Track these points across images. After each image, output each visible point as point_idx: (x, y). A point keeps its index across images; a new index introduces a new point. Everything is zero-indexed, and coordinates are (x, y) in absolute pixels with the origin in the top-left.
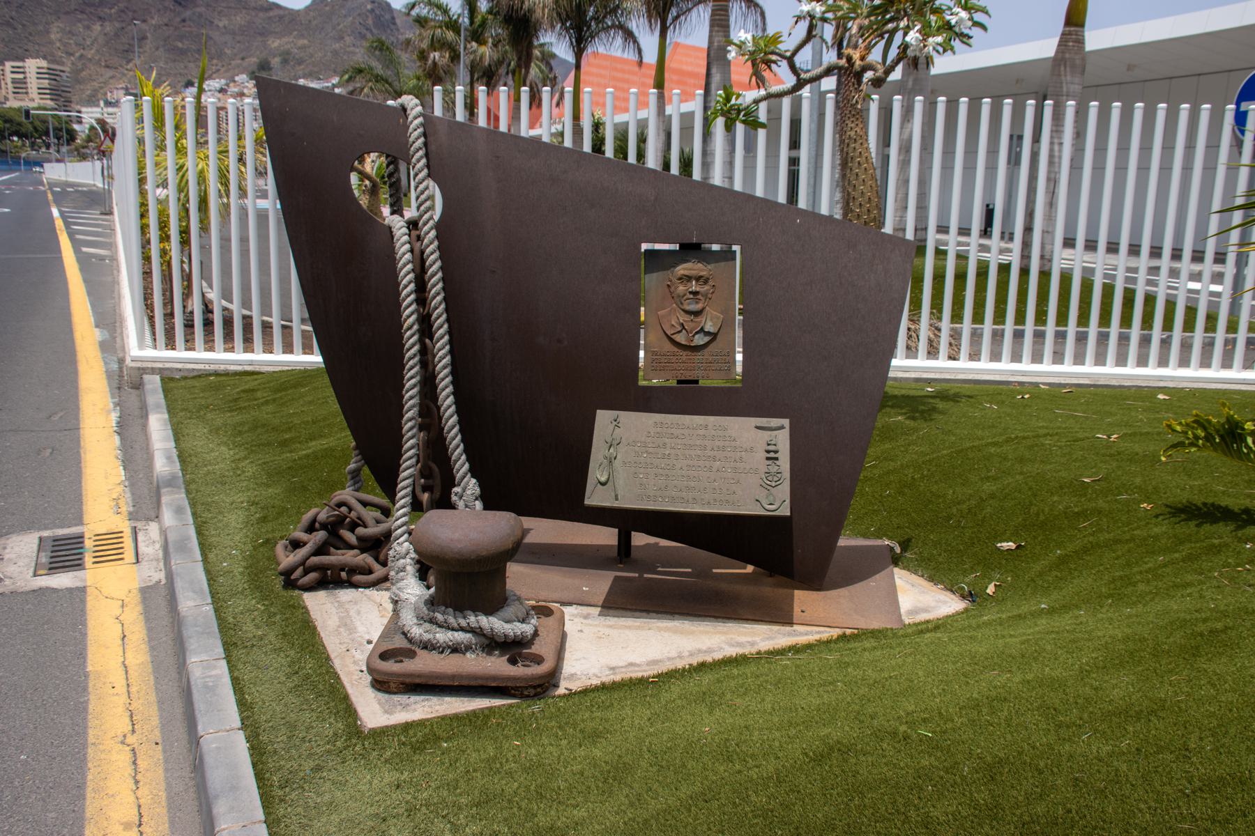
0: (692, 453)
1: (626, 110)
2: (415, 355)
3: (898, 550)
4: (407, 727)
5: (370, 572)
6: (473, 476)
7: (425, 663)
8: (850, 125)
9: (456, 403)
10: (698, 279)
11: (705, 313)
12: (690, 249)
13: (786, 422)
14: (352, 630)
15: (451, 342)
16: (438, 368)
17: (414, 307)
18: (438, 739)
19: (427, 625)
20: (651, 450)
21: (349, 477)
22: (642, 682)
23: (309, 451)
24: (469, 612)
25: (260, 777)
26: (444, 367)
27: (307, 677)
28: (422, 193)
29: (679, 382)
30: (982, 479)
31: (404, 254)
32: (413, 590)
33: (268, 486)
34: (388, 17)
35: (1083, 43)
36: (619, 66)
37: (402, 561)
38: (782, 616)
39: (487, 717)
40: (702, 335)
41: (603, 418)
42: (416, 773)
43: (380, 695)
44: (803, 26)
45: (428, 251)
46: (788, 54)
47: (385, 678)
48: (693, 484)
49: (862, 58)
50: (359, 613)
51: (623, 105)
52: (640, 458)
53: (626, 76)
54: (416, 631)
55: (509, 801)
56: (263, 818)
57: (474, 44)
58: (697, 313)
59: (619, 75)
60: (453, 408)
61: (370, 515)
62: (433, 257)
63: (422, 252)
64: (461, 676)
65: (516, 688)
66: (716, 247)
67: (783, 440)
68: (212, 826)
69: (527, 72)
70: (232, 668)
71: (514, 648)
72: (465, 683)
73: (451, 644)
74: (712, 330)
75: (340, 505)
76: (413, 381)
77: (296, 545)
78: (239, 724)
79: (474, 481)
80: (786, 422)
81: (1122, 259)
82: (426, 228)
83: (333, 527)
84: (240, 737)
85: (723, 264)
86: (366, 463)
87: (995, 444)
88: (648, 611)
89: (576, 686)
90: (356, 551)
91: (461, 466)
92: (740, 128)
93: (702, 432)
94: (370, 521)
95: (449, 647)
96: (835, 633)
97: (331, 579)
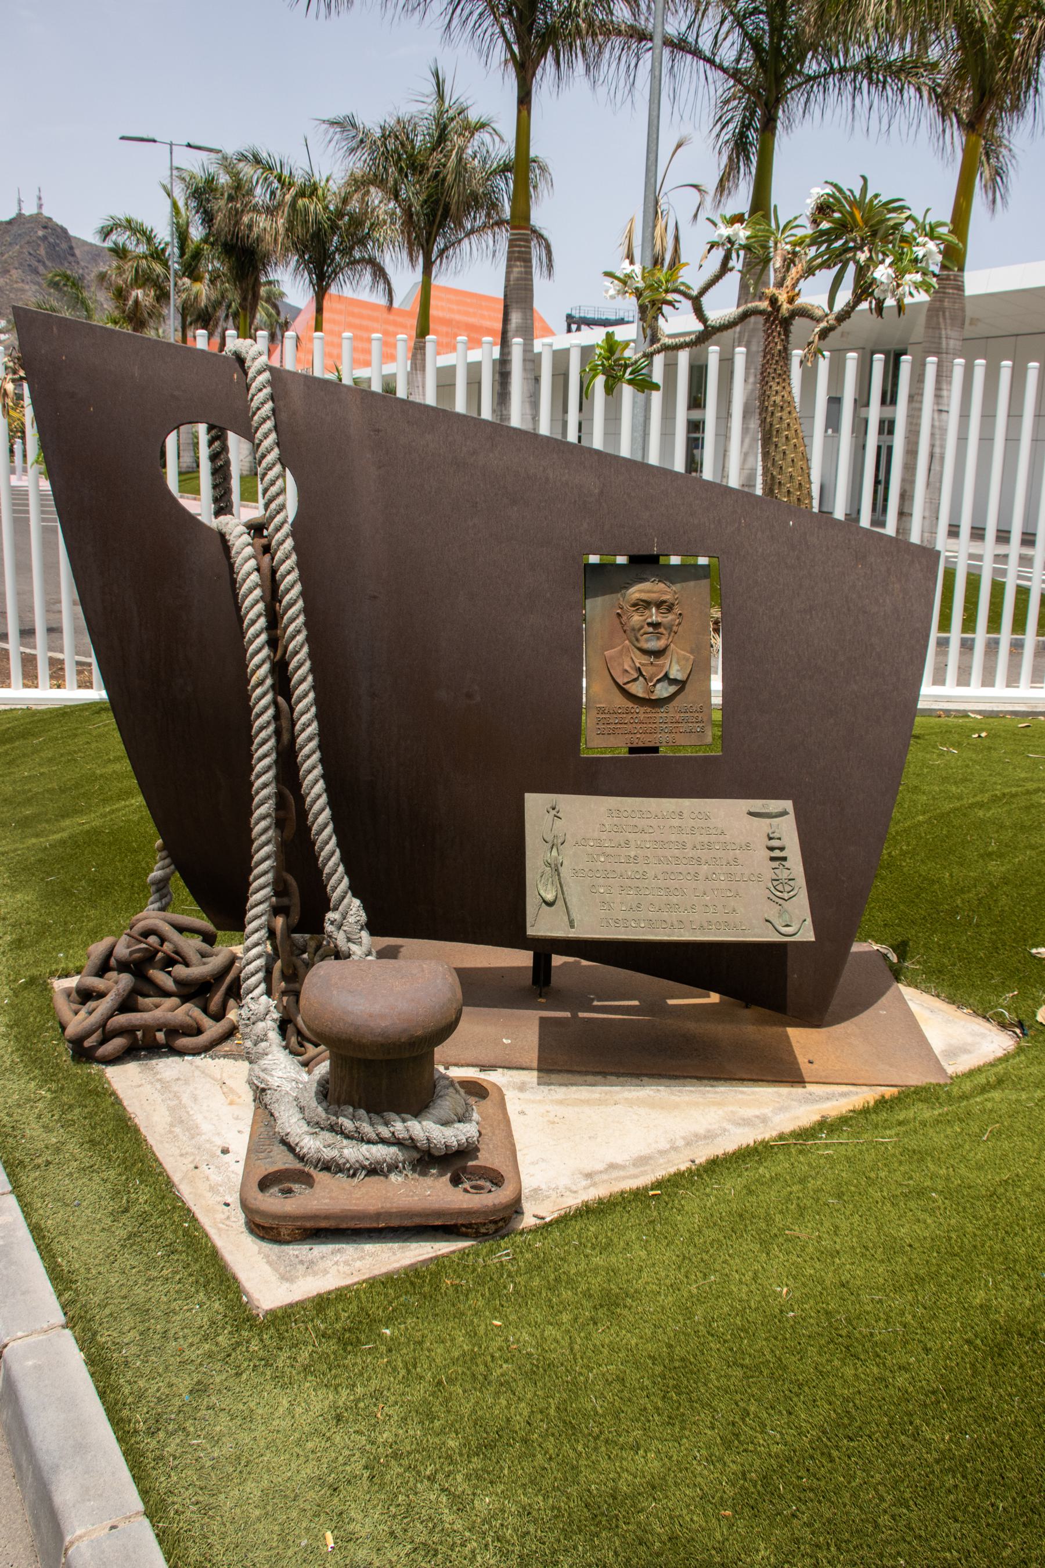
0: (668, 853)
1: (368, 364)
2: (268, 723)
3: (894, 958)
4: (322, 1303)
5: (199, 1031)
6: (354, 895)
7: (328, 1196)
8: (775, 388)
9: (327, 790)
10: (659, 605)
11: (668, 653)
12: (645, 563)
13: (788, 805)
14: (193, 1131)
15: (317, 701)
16: (300, 740)
17: (265, 652)
18: (374, 1322)
19: (327, 1136)
20: (608, 851)
21: (153, 889)
22: (638, 1195)
23: (65, 835)
24: (392, 1116)
25: (117, 1422)
26: (310, 739)
27: (145, 1217)
28: (273, 483)
29: (632, 750)
30: (981, 856)
31: (249, 574)
32: (292, 1078)
33: (14, 890)
34: (64, 246)
35: (963, 291)
36: (356, 310)
37: (261, 1025)
38: (785, 1072)
39: (436, 1275)
40: (665, 684)
41: (535, 803)
42: (359, 1390)
43: (267, 1247)
44: (719, 254)
45: (283, 569)
46: (695, 293)
47: (274, 1223)
48: (675, 899)
49: (791, 301)
50: (195, 1099)
51: (362, 357)
52: (604, 865)
53: (365, 323)
54: (311, 1144)
55: (525, 1441)
56: (140, 1507)
57: (186, 280)
58: (658, 654)
59: (357, 321)
60: (324, 799)
61: (191, 945)
62: (290, 578)
63: (274, 571)
64: (389, 1214)
65: (469, 1226)
66: (675, 560)
67: (788, 831)
68: (58, 1533)
69: (253, 317)
70: (27, 1209)
71: (455, 1162)
72: (395, 1223)
73: (362, 1161)
74: (680, 676)
75: (146, 933)
76: (267, 761)
77: (85, 995)
78: (60, 1318)
79: (357, 902)
80: (788, 805)
81: (964, 545)
82: (279, 536)
83: (138, 968)
84: (67, 1341)
85: (692, 584)
86: (178, 868)
87: (981, 805)
88: (604, 1074)
89: (549, 1211)
90: (175, 1000)
91: (338, 883)
92: (627, 391)
93: (676, 822)
94: (193, 957)
95: (364, 1167)
96: (862, 1097)
97: (144, 1046)
